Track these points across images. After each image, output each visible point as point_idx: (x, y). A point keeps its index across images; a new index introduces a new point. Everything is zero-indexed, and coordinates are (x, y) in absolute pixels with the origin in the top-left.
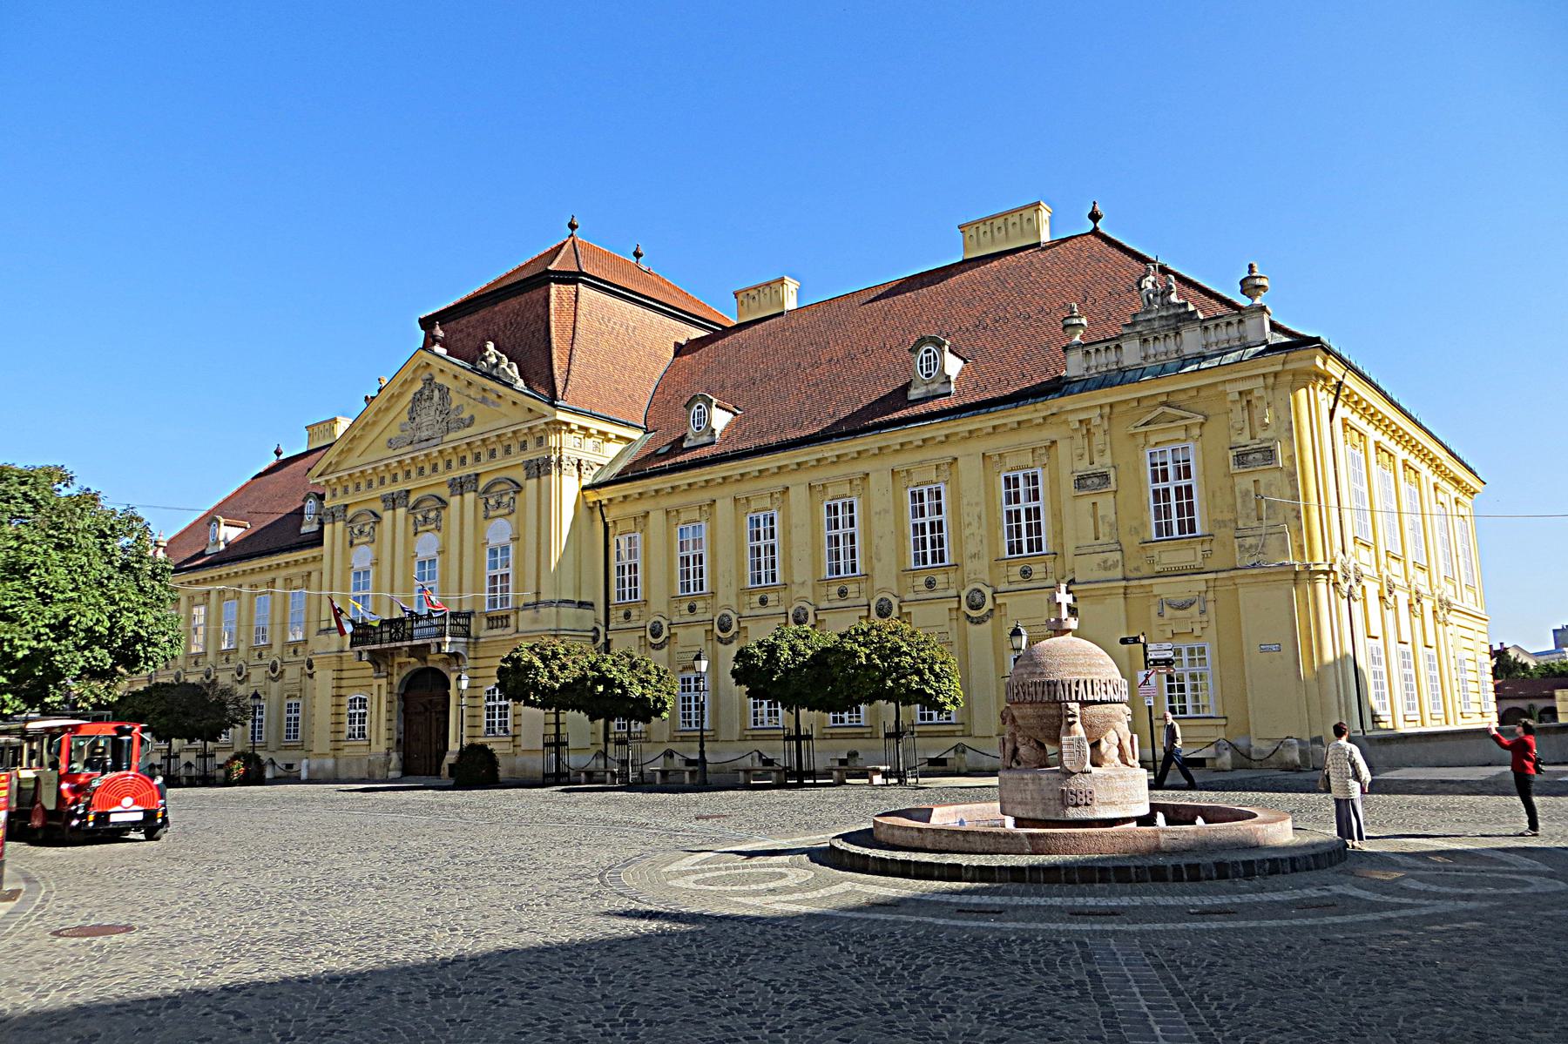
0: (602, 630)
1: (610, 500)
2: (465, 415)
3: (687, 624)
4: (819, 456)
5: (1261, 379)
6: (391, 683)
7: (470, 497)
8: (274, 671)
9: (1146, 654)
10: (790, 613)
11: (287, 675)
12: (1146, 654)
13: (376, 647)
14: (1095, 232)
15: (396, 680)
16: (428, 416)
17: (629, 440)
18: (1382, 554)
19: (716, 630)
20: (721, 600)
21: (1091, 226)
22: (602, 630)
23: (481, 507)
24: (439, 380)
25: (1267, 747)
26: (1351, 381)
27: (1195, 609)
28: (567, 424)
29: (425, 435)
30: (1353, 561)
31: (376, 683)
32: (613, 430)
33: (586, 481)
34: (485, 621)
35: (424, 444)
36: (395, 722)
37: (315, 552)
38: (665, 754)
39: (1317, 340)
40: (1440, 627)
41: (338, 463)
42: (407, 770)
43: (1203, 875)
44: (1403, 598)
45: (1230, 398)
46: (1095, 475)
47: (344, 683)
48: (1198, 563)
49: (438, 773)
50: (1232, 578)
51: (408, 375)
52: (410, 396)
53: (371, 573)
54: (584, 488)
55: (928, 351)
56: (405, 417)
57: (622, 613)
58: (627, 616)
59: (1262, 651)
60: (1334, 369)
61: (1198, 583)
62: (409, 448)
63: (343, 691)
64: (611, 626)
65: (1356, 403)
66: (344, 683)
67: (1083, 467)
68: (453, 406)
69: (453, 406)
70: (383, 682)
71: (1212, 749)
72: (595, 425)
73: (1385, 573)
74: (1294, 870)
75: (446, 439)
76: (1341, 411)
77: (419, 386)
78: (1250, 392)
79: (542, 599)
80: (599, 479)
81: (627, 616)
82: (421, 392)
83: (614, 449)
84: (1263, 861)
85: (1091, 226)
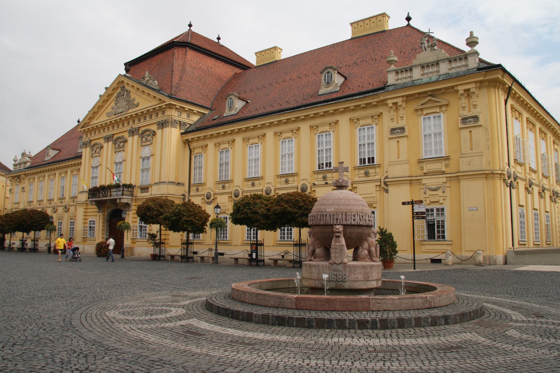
0: (187, 195)
1: (192, 139)
2: (136, 103)
3: (222, 194)
4: (204, 135)
5: (474, 84)
6: (104, 215)
7: (136, 137)
8: (66, 208)
9: (413, 210)
10: (264, 189)
11: (70, 210)
12: (413, 210)
13: (97, 199)
14: (408, 25)
15: (106, 214)
16: (122, 103)
17: (204, 114)
18: (541, 175)
19: (205, 199)
20: (236, 183)
21: (406, 23)
22: (187, 195)
23: (140, 141)
24: (127, 88)
25: (469, 254)
26: (515, 88)
27: (439, 192)
28: (175, 105)
29: (120, 110)
30: (529, 177)
31: (98, 214)
32: (196, 109)
33: (183, 131)
34: (139, 190)
35: (120, 115)
36: (105, 231)
37: (79, 161)
38: (208, 250)
39: (500, 65)
40: (553, 204)
41: (88, 123)
42: (429, 239)
43: (389, 325)
44: (536, 190)
45: (460, 92)
46: (399, 128)
47: (88, 214)
48: (444, 169)
49: (434, 238)
50: (458, 176)
51: (115, 85)
52: (115, 95)
53: (101, 168)
54: (182, 134)
55: (328, 73)
56: (113, 104)
57: (195, 188)
58: (197, 190)
59: (470, 210)
60: (508, 82)
61: (442, 179)
62: (114, 116)
63: (87, 217)
64: (191, 194)
65: (529, 108)
66: (88, 214)
67: (394, 125)
68: (132, 98)
69: (132, 98)
70: (101, 214)
71: (444, 255)
72: (188, 107)
73: (529, 177)
74: (447, 323)
75: (128, 112)
76: (510, 102)
77: (119, 90)
78: (469, 90)
79: (410, 206)
80: (188, 130)
81: (197, 190)
82: (120, 93)
83: (195, 118)
84: (427, 318)
85: (406, 23)
